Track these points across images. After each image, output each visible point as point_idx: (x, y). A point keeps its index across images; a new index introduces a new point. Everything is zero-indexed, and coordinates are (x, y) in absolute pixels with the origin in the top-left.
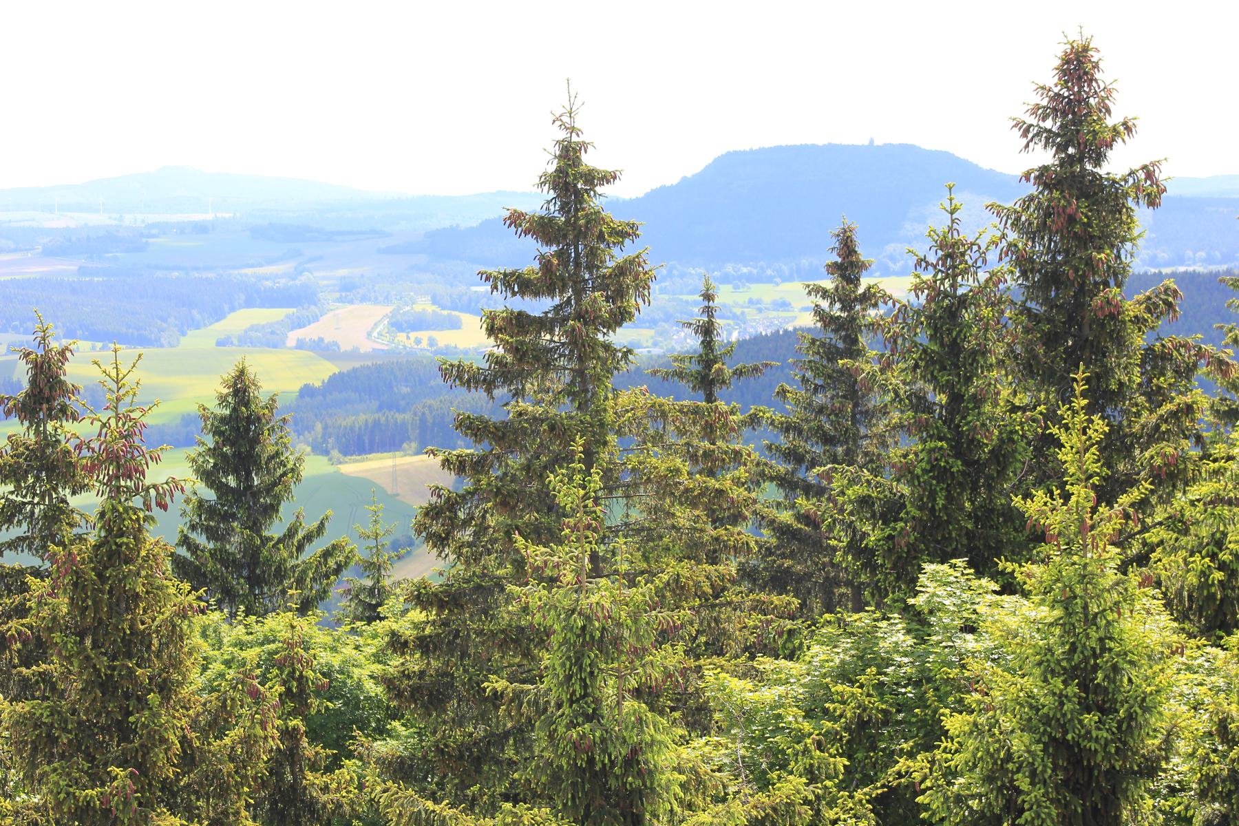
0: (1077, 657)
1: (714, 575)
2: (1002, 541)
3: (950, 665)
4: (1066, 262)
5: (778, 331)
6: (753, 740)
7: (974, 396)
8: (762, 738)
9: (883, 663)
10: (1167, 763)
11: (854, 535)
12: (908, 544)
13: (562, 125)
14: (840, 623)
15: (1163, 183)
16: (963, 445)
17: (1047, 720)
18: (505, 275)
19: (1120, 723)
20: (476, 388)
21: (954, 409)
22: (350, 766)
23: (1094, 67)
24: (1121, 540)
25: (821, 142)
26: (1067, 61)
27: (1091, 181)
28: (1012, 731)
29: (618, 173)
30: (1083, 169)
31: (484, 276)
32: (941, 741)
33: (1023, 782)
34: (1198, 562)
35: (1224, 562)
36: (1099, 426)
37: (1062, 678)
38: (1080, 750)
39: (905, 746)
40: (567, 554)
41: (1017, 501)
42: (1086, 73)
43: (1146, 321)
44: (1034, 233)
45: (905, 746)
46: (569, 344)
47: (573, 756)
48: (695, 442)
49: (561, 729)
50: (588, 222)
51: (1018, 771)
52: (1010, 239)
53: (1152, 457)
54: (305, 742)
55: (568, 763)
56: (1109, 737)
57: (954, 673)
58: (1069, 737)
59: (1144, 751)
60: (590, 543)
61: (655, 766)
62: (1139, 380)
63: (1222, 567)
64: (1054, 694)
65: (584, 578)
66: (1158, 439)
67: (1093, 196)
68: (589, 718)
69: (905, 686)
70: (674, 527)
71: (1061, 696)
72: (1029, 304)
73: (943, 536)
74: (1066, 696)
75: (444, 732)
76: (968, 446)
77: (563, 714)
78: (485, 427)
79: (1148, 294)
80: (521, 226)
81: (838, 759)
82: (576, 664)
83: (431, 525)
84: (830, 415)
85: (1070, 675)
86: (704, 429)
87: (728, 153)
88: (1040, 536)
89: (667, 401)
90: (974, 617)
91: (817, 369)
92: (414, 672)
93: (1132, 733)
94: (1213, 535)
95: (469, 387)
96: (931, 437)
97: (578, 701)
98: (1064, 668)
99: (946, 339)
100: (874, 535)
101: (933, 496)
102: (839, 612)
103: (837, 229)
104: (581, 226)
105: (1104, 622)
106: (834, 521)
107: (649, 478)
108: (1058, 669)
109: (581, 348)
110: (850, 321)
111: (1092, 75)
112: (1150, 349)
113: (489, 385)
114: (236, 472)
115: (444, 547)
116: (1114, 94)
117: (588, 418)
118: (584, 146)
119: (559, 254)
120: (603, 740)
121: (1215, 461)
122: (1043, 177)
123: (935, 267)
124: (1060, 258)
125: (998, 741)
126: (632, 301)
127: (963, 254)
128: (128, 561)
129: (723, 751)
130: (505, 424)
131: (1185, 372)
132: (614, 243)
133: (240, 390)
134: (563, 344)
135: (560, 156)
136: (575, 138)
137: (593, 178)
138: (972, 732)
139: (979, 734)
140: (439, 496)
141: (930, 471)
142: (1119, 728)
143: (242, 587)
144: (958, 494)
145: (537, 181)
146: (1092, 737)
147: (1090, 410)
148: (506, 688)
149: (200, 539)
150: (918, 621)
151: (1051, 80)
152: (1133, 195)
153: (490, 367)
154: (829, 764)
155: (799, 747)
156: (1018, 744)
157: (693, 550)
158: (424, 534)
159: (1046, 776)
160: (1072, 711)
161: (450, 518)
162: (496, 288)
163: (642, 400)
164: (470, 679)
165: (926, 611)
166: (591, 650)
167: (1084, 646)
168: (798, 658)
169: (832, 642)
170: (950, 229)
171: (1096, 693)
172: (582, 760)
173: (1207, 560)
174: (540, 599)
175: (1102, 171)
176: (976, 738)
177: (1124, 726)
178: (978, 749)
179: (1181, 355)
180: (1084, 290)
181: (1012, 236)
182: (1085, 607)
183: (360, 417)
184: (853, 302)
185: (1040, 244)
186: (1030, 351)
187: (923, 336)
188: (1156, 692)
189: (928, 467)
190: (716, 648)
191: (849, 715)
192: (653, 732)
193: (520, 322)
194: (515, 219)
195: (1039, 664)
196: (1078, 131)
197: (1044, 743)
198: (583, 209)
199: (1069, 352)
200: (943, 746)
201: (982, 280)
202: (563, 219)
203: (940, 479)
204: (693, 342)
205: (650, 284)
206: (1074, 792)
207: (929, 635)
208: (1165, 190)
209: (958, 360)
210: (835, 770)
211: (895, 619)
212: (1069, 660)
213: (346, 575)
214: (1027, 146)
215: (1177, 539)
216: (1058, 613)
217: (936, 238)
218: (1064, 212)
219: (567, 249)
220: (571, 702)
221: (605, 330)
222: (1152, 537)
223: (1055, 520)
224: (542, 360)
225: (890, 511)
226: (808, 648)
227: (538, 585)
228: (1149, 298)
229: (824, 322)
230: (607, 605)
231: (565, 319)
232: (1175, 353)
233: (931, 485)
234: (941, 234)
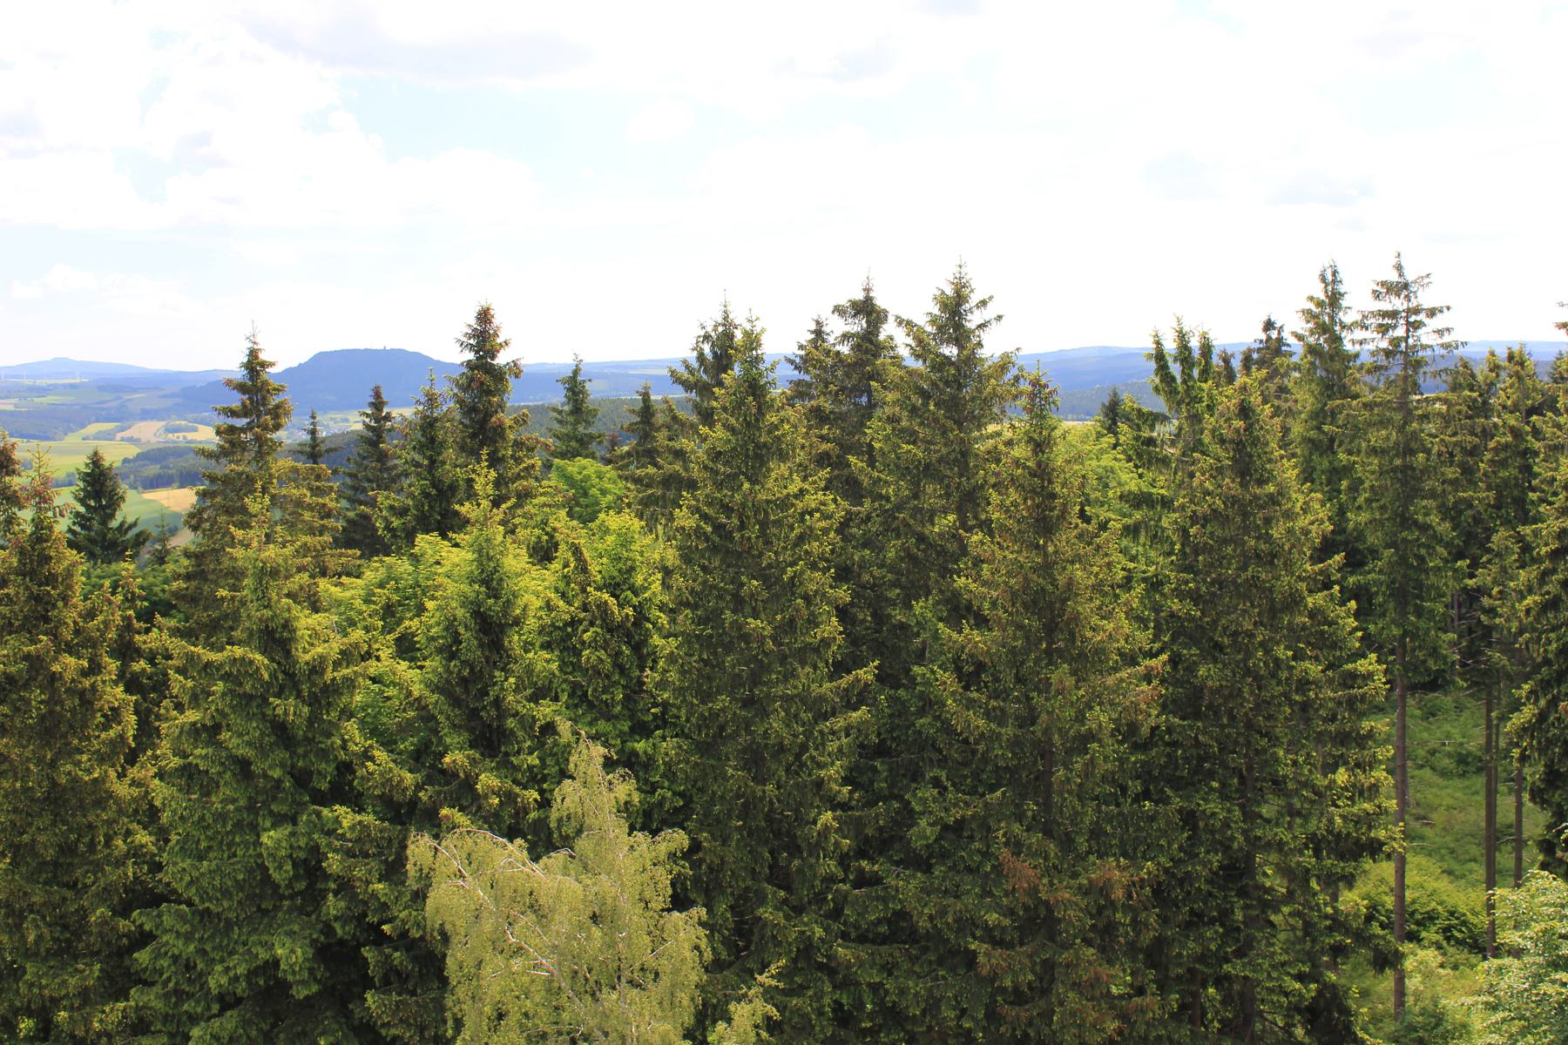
6: (341, 614)
14: (381, 561)
17: (472, 603)
22: (155, 632)
24: (503, 523)
25: (362, 347)
33: (461, 630)
36: (493, 474)
41: (457, 507)
54: (135, 621)
63: (547, 534)
68: (265, 607)
88: (468, 521)
89: (299, 465)
100: (396, 523)
101: (423, 505)
112: (515, 441)
114: (94, 498)
122: (469, 363)
126: (283, 420)
128: (47, 541)
130: (226, 476)
131: (531, 449)
133: (96, 460)
137: (264, 365)
143: (98, 551)
147: (489, 467)
149: (77, 528)
150: (416, 559)
151: (473, 322)
156: (460, 613)
157: (312, 531)
169: (377, 570)
175: (495, 362)
181: (456, 391)
183: (153, 470)
186: (463, 439)
187: (419, 435)
190: (324, 574)
194: (229, 383)
204: (306, 437)
206: (484, 634)
213: (147, 544)
216: (476, 556)
222: (516, 521)
223: (472, 516)
224: (243, 447)
225: (402, 512)
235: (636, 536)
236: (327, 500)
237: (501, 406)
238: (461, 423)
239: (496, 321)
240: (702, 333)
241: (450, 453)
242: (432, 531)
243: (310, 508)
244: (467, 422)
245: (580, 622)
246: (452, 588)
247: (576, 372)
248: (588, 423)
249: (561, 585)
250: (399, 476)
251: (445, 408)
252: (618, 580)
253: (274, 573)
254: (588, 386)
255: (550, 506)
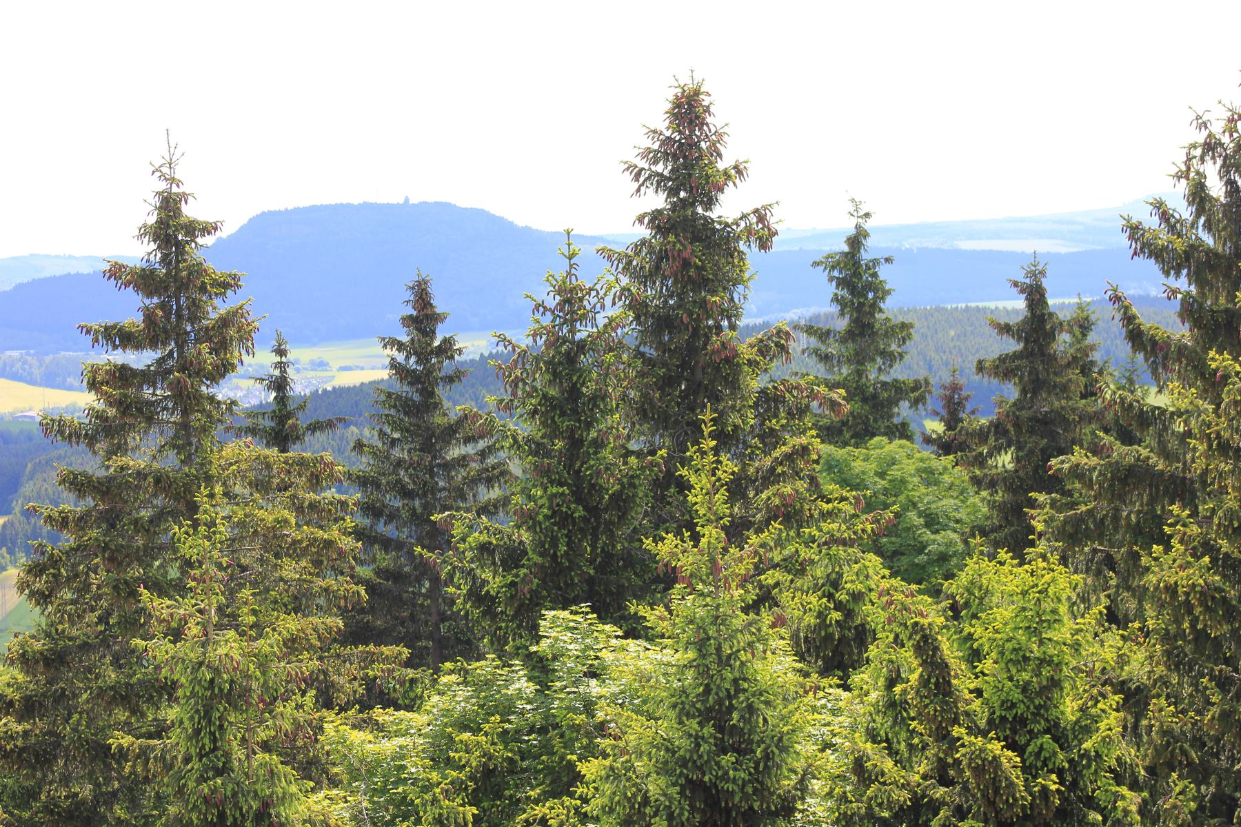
0: (711, 699)
1: (321, 628)
2: (623, 585)
3: (574, 710)
4: (679, 307)
5: (317, 391)
7: (595, 441)
8: (384, 791)
9: (506, 709)
10: (803, 804)
11: (474, 583)
12: (531, 591)
13: (162, 175)
15: (774, 226)
16: (583, 490)
17: (684, 763)
18: (106, 328)
19: (757, 764)
20: (78, 443)
21: (573, 455)
23: (705, 111)
25: (356, 200)
26: (677, 104)
27: (703, 225)
28: (648, 775)
29: (219, 224)
30: (695, 213)
31: (85, 330)
32: (577, 787)
34: (814, 600)
35: (841, 602)
37: (698, 720)
38: (718, 791)
39: (532, 793)
40: (193, 606)
41: (648, 543)
42: (697, 117)
43: (758, 363)
44: (646, 277)
45: (532, 793)
46: (174, 396)
47: (203, 811)
48: (301, 494)
49: (191, 784)
50: (190, 274)
51: (656, 814)
52: (623, 284)
53: (769, 498)
55: (198, 818)
56: (747, 778)
57: (580, 719)
58: (706, 779)
59: (781, 792)
60: (217, 594)
61: (286, 819)
62: (752, 422)
63: (839, 606)
64: (691, 735)
65: (211, 629)
66: (773, 482)
67: (705, 240)
68: (219, 772)
69: (529, 734)
70: (282, 579)
71: (697, 737)
72: (642, 349)
73: (566, 583)
74: (703, 738)
75: (49, 793)
76: (589, 491)
77: (192, 768)
78: (89, 482)
79: (760, 336)
80: (121, 278)
81: (468, 808)
82: (205, 715)
83: (34, 582)
84: (409, 468)
85: (705, 716)
86: (309, 480)
87: (263, 213)
88: (669, 577)
90: (596, 662)
91: (395, 422)
92: (18, 733)
93: (769, 775)
94: (828, 575)
95: (70, 441)
96: (552, 482)
97: (207, 755)
98: (698, 710)
99: (565, 384)
100: (494, 581)
101: (554, 542)
102: (459, 661)
103: (411, 279)
104: (183, 278)
105: (738, 663)
106: (454, 568)
107: (256, 531)
108: (692, 711)
109: (186, 400)
110: (427, 375)
111: (704, 119)
113: (91, 439)
115: (47, 605)
116: (725, 138)
117: (193, 471)
118: (185, 197)
119: (162, 306)
120: (235, 794)
121: (829, 501)
122: (654, 219)
123: (553, 312)
124: (671, 302)
125: (635, 785)
126: (236, 351)
127: (581, 300)
129: (342, 805)
132: (216, 294)
134: (166, 398)
135: (161, 207)
136: (175, 189)
137: (194, 229)
138: (608, 777)
139: (615, 779)
140: (43, 553)
141: (551, 517)
142: (756, 768)
144: (579, 540)
145: (137, 232)
146: (729, 778)
148: (133, 744)
150: (541, 669)
151: (662, 123)
152: (744, 238)
153: (90, 421)
154: (459, 813)
155: (428, 797)
156: (654, 787)
158: (27, 592)
159: (684, 819)
160: (709, 752)
161: (54, 575)
162: (97, 341)
163: (246, 453)
164: (80, 737)
165: (550, 657)
166: (220, 703)
167: (719, 687)
168: (419, 708)
170: (569, 274)
171: (731, 735)
172: (213, 814)
173: (825, 600)
174: (167, 652)
175: (714, 214)
176: (612, 783)
177: (762, 765)
178: (614, 793)
179: (793, 396)
180: (699, 335)
181: (625, 281)
182: (719, 649)
184: (429, 354)
185: (652, 289)
187: (540, 380)
188: (793, 731)
189: (550, 513)
191: (474, 764)
192: (284, 784)
193: (123, 375)
194: (116, 272)
195: (674, 706)
196: (690, 175)
197: (681, 785)
198: (185, 261)
199: (685, 395)
200: (579, 791)
201: (601, 326)
202: (164, 271)
203: (561, 525)
205: (253, 334)
207: (552, 681)
208: (776, 233)
209: (577, 406)
210: (464, 818)
211: (517, 665)
212: (703, 702)
214: (638, 190)
215: (792, 581)
216: (691, 655)
217: (554, 283)
218: (679, 255)
219: (168, 301)
220: (201, 757)
221: (208, 383)
224: (146, 413)
225: (512, 557)
226: (429, 697)
227: (164, 638)
228: (761, 341)
229: (401, 375)
230: (237, 657)
231: (169, 371)
232: (787, 395)
233: (553, 531)
234: (559, 279)
235: (1063, 609)
236: (334, 533)
237: (731, 313)
238: (639, 354)
239: (715, 121)
240: (1201, 137)
241: (615, 422)
242: (576, 601)
243: (295, 550)
244: (650, 351)
245: (935, 807)
246: (637, 732)
247: (856, 241)
248: (890, 358)
249: (883, 724)
250: (473, 482)
251: (601, 320)
252: (1021, 709)
253: (236, 696)
254: (883, 272)
255: (844, 543)
